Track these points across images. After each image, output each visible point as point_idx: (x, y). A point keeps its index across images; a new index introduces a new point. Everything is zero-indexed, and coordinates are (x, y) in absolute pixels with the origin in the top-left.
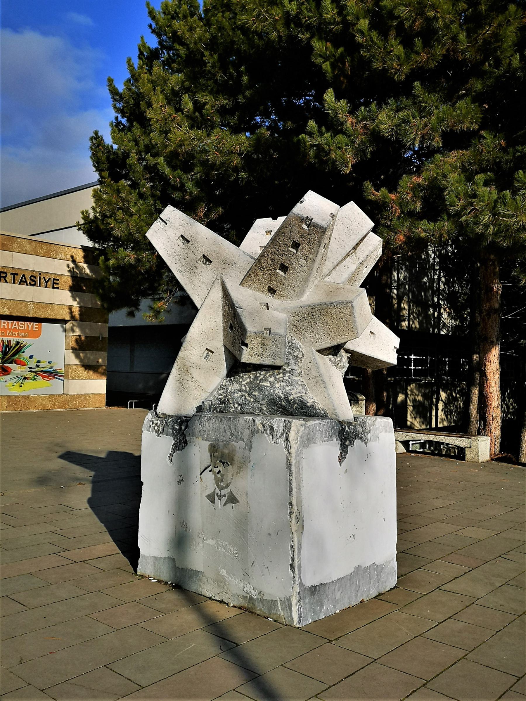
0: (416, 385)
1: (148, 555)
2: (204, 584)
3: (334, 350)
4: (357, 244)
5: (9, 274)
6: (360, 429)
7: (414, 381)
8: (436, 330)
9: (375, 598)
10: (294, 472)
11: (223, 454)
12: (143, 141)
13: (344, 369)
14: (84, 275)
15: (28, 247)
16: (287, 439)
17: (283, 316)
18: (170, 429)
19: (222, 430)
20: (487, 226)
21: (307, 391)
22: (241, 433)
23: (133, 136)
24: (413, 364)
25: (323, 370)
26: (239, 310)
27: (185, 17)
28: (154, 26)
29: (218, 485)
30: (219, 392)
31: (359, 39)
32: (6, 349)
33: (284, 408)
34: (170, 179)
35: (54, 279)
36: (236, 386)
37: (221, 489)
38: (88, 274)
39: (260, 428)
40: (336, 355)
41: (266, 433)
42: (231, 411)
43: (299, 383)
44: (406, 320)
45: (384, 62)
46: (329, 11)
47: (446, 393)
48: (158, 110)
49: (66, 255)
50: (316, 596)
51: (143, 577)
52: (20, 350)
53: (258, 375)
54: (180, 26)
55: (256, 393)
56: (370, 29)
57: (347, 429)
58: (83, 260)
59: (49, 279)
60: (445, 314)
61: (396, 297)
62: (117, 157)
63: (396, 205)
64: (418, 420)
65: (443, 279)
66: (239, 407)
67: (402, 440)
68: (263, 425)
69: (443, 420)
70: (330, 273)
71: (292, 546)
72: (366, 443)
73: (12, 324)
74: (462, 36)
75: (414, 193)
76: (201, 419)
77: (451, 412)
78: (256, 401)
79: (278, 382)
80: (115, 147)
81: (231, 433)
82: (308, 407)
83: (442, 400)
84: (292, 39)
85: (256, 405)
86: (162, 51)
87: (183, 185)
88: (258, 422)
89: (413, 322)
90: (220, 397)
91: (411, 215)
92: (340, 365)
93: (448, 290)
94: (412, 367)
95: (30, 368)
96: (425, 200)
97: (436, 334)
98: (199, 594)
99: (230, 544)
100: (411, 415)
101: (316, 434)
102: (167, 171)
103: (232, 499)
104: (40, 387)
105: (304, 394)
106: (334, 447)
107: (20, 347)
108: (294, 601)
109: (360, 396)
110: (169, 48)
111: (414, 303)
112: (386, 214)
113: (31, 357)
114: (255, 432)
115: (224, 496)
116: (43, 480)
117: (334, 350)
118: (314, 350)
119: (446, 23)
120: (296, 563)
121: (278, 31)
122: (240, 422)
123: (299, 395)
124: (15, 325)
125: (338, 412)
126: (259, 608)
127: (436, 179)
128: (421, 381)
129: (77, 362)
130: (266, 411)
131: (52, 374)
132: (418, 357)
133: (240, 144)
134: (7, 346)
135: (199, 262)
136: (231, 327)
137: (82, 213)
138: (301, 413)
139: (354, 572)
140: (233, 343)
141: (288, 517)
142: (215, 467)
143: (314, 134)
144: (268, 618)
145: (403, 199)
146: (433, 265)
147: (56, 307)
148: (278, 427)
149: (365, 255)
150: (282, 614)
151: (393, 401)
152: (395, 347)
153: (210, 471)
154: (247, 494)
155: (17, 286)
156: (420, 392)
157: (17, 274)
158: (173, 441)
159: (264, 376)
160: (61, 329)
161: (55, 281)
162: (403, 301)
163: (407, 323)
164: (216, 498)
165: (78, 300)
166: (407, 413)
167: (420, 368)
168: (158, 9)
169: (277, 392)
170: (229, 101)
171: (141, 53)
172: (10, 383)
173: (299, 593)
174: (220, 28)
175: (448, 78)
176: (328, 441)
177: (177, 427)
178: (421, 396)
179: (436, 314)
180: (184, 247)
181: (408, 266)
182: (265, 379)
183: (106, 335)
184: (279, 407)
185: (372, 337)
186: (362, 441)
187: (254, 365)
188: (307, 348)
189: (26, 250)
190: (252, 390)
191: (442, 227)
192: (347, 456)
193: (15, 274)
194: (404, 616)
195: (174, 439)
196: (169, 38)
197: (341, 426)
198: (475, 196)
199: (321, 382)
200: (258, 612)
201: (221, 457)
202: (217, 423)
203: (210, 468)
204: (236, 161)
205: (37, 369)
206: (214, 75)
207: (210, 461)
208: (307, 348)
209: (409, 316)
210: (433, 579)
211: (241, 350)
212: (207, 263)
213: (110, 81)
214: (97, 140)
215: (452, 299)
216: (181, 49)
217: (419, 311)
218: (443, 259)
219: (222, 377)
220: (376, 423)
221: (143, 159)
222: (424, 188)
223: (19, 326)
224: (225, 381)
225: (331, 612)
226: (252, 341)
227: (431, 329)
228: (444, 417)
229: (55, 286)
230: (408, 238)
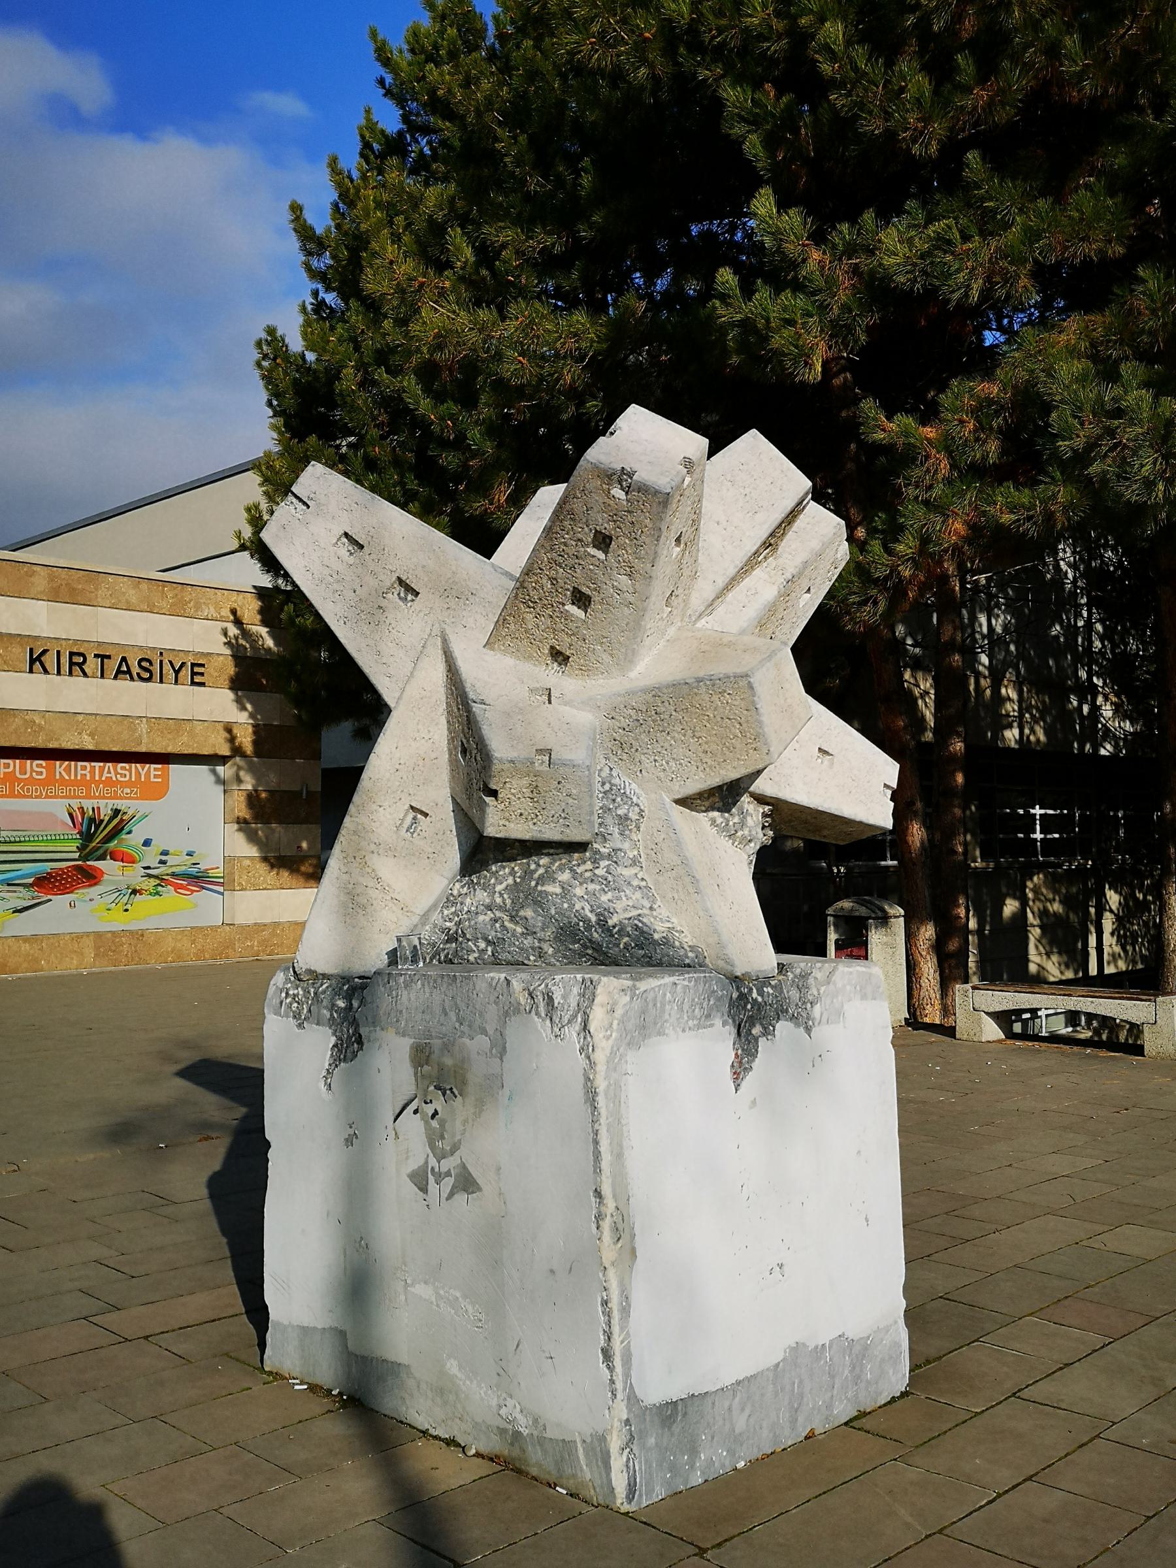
0: (1045, 876)
1: (286, 1323)
2: (412, 1395)
3: (722, 798)
4: (772, 535)
5: (90, 658)
6: (794, 994)
7: (1041, 867)
8: (1088, 746)
9: (846, 1424)
10: (603, 1111)
11: (441, 1068)
12: (370, 343)
13: (752, 845)
14: (262, 652)
15: (132, 595)
16: (585, 1027)
17: (586, 719)
18: (325, 1008)
19: (437, 1010)
20: (1149, 484)
21: (654, 902)
22: (481, 1015)
23: (348, 330)
24: (1038, 827)
25: (691, 848)
26: (476, 708)
27: (453, 55)
28: (389, 79)
29: (432, 1147)
30: (446, 912)
31: (826, 68)
32: (89, 828)
33: (597, 947)
34: (432, 423)
35: (193, 665)
36: (482, 896)
37: (440, 1157)
38: (270, 649)
39: (523, 1002)
40: (729, 811)
41: (537, 1014)
42: (471, 958)
43: (635, 883)
44: (1015, 724)
45: (888, 116)
46: (758, 11)
47: (1121, 894)
48: (392, 266)
49: (218, 608)
50: (676, 1429)
51: (277, 1376)
52: (123, 829)
53: (533, 867)
54: (441, 74)
55: (528, 913)
56: (848, 43)
57: (755, 995)
58: (259, 617)
59: (183, 664)
60: (1108, 707)
61: (987, 673)
62: (316, 378)
63: (938, 452)
64: (1055, 958)
65: (1099, 627)
66: (490, 949)
67: (991, 1010)
68: (530, 994)
69: (1114, 958)
70: (711, 606)
71: (605, 1303)
72: (808, 1030)
73: (102, 770)
74: (1072, 42)
75: (977, 419)
76: (392, 983)
77: (1134, 936)
78: (529, 932)
79: (581, 884)
80: (311, 357)
81: (458, 1014)
82: (656, 943)
83: (1111, 911)
84: (683, 83)
85: (528, 942)
86: (413, 137)
87: (461, 437)
88: (517, 985)
89: (1033, 731)
90: (448, 924)
91: (978, 472)
92: (740, 833)
93: (1112, 651)
94: (1038, 836)
95: (145, 868)
96: (1008, 436)
97: (1088, 755)
98: (401, 1422)
99: (465, 1297)
100: (1037, 947)
101: (663, 1010)
102: (424, 406)
103: (467, 1183)
104: (169, 913)
105: (646, 911)
106: (721, 1042)
107: (122, 820)
108: (615, 1443)
109: (891, 906)
110: (426, 130)
111: (1031, 684)
112: (916, 473)
113: (147, 843)
114: (511, 1011)
115: (448, 1174)
116: (121, 1133)
117: (725, 796)
118: (668, 800)
119: (1031, 16)
120: (617, 1346)
121: (652, 66)
122: (478, 988)
123: (635, 913)
124: (109, 772)
125: (733, 952)
126: (538, 1461)
127: (1031, 384)
128: (1060, 866)
129: (253, 851)
130: (553, 956)
131: (197, 880)
132: (1051, 812)
133: (576, 335)
134: (92, 820)
135: (390, 596)
136: (464, 751)
137: (248, 510)
138: (639, 960)
139: (784, 1360)
140: (468, 789)
141: (594, 1226)
142: (426, 1103)
143: (729, 297)
144: (556, 1485)
145: (953, 438)
146: (1073, 595)
147: (199, 727)
148: (564, 997)
149: (799, 560)
150: (588, 1476)
151: (991, 916)
152: (886, 786)
153: (416, 1112)
154: (499, 1169)
155: (108, 682)
156: (1056, 891)
157: (109, 657)
158: (333, 1040)
159: (547, 867)
160: (212, 778)
161: (196, 669)
162: (1006, 682)
163: (1016, 732)
164: (431, 1178)
165: (249, 706)
166: (1027, 945)
167: (1057, 836)
168: (398, 44)
169: (577, 907)
170: (559, 238)
171: (367, 145)
172: (100, 903)
173: (627, 1422)
174: (533, 75)
175: (1046, 142)
176: (699, 1027)
177: (341, 1004)
178: (1061, 902)
179: (1086, 709)
180: (351, 560)
181: (1011, 599)
182: (548, 877)
183: (317, 787)
184: (584, 946)
185: (826, 762)
186: (798, 1025)
187: (522, 842)
188: (652, 792)
189: (128, 602)
190: (518, 905)
191: (1049, 498)
192: (755, 1065)
193: (103, 657)
194: (913, 1474)
195: (334, 1034)
196: (425, 105)
197: (738, 988)
198: (1118, 413)
199: (688, 880)
200: (534, 1471)
201: (442, 1076)
202: (427, 990)
203: (413, 1106)
204: (570, 374)
205: (163, 870)
206: (524, 182)
207: (414, 1087)
208: (652, 792)
209: (1021, 716)
210: (1005, 1369)
211: (482, 806)
212: (410, 597)
213: (296, 209)
214: (272, 345)
215: (1120, 671)
216: (447, 128)
217: (1043, 702)
218: (1095, 578)
219: (450, 875)
220: (837, 977)
221: (374, 383)
222: (1002, 406)
223: (117, 773)
224: (458, 885)
225: (723, 1466)
226: (512, 788)
227: (1076, 745)
228: (1117, 949)
229: (197, 679)
230: (973, 527)
